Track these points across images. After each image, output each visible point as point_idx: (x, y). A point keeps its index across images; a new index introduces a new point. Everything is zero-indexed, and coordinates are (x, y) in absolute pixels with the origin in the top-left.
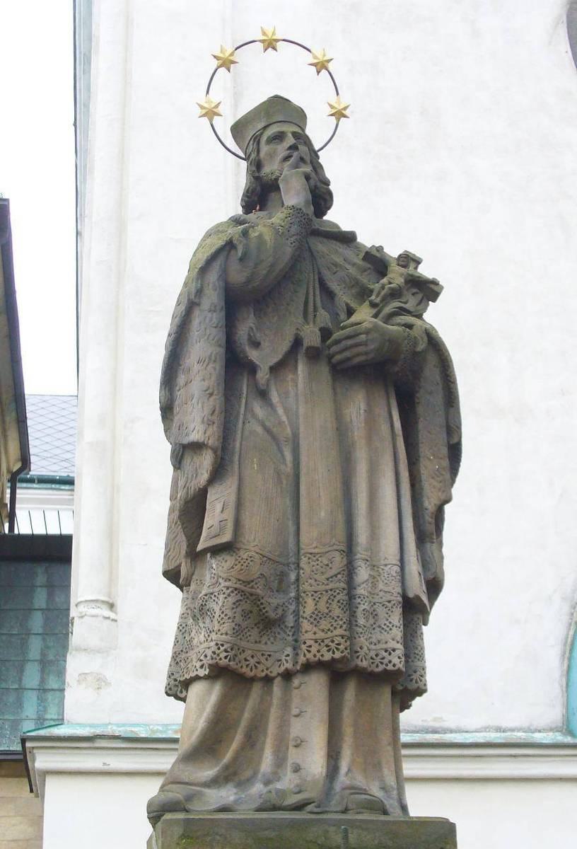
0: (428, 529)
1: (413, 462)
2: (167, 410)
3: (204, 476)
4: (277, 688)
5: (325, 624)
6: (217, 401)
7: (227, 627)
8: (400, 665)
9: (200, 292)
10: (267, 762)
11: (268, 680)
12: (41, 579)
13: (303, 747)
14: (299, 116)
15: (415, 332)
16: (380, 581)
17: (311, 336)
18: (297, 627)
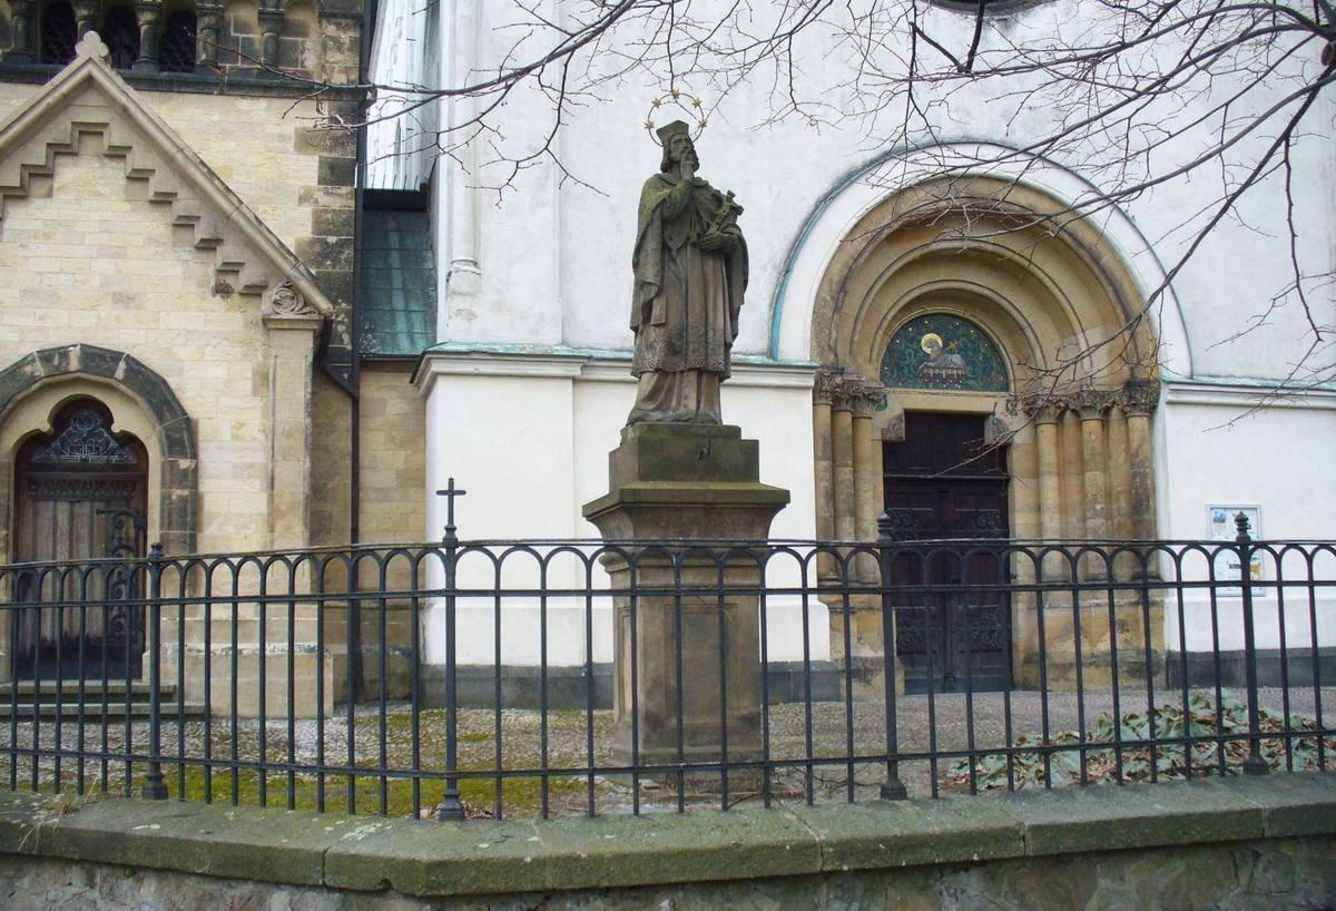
0: (734, 315)
1: (730, 286)
2: (636, 265)
3: (653, 295)
4: (678, 376)
5: (697, 354)
6: (659, 267)
7: (662, 354)
8: (723, 368)
9: (652, 220)
10: (674, 403)
11: (675, 373)
12: (392, 225)
13: (688, 400)
14: (686, 126)
15: (735, 236)
16: (715, 338)
17: (694, 238)
18: (687, 354)
